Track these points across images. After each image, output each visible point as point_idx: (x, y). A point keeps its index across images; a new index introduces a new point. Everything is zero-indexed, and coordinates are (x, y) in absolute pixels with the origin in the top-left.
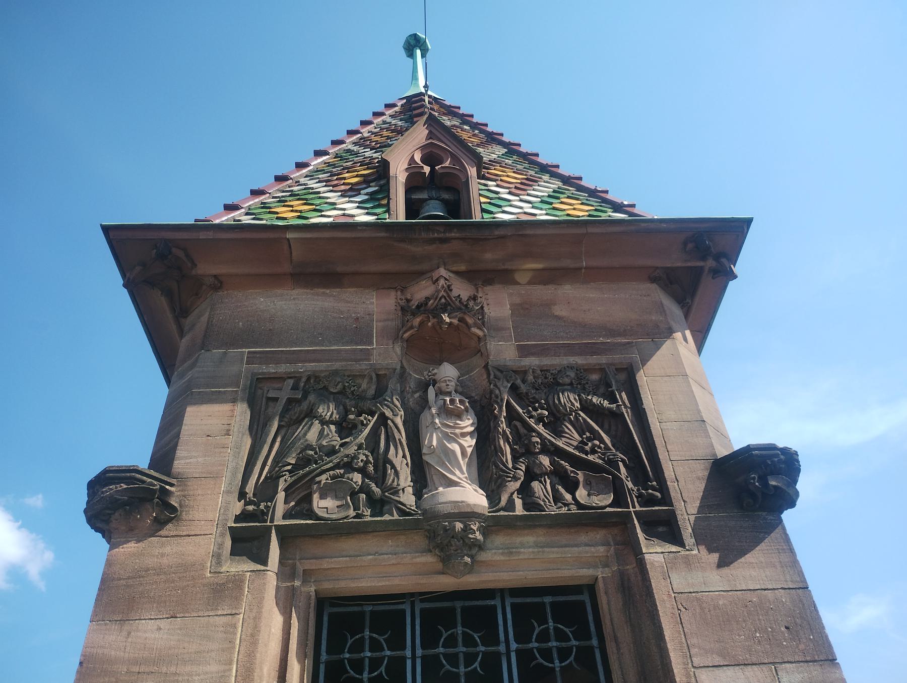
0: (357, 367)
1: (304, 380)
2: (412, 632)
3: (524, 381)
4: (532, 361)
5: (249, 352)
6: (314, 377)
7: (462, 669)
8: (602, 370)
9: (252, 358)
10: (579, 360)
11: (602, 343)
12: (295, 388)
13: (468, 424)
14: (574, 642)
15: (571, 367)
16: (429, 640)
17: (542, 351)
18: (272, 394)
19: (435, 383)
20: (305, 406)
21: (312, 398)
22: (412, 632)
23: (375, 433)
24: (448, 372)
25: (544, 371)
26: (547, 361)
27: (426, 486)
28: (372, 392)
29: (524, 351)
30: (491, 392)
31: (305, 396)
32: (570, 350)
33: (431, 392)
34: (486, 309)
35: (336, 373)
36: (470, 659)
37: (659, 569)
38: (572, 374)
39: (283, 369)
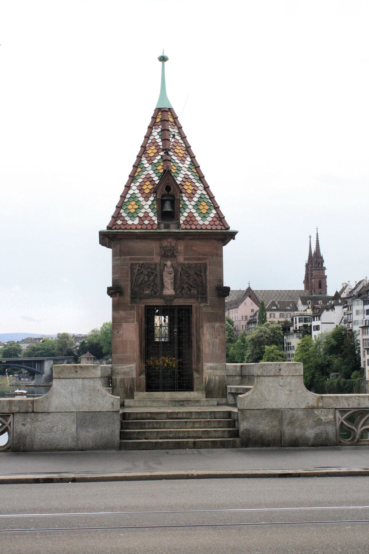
0: (151, 262)
1: (140, 265)
2: (176, 312)
3: (184, 266)
4: (186, 262)
5: (130, 258)
6: (143, 264)
7: (150, 326)
8: (200, 264)
9: (131, 259)
10: (196, 262)
11: (202, 258)
12: (139, 267)
13: (221, 435)
14: (180, 315)
15: (194, 264)
16: (179, 313)
17: (189, 259)
18: (135, 267)
19: (166, 265)
20: (141, 271)
21: (143, 269)
22: (176, 312)
23: (155, 277)
24: (169, 263)
25: (188, 264)
26: (189, 262)
27: (164, 288)
28: (154, 268)
29: (185, 259)
30: (177, 269)
31: (141, 269)
32: (195, 259)
33: (166, 267)
34: (178, 248)
35: (147, 263)
36: (182, 314)
37: (70, 387)
38: (194, 265)
39: (137, 262)
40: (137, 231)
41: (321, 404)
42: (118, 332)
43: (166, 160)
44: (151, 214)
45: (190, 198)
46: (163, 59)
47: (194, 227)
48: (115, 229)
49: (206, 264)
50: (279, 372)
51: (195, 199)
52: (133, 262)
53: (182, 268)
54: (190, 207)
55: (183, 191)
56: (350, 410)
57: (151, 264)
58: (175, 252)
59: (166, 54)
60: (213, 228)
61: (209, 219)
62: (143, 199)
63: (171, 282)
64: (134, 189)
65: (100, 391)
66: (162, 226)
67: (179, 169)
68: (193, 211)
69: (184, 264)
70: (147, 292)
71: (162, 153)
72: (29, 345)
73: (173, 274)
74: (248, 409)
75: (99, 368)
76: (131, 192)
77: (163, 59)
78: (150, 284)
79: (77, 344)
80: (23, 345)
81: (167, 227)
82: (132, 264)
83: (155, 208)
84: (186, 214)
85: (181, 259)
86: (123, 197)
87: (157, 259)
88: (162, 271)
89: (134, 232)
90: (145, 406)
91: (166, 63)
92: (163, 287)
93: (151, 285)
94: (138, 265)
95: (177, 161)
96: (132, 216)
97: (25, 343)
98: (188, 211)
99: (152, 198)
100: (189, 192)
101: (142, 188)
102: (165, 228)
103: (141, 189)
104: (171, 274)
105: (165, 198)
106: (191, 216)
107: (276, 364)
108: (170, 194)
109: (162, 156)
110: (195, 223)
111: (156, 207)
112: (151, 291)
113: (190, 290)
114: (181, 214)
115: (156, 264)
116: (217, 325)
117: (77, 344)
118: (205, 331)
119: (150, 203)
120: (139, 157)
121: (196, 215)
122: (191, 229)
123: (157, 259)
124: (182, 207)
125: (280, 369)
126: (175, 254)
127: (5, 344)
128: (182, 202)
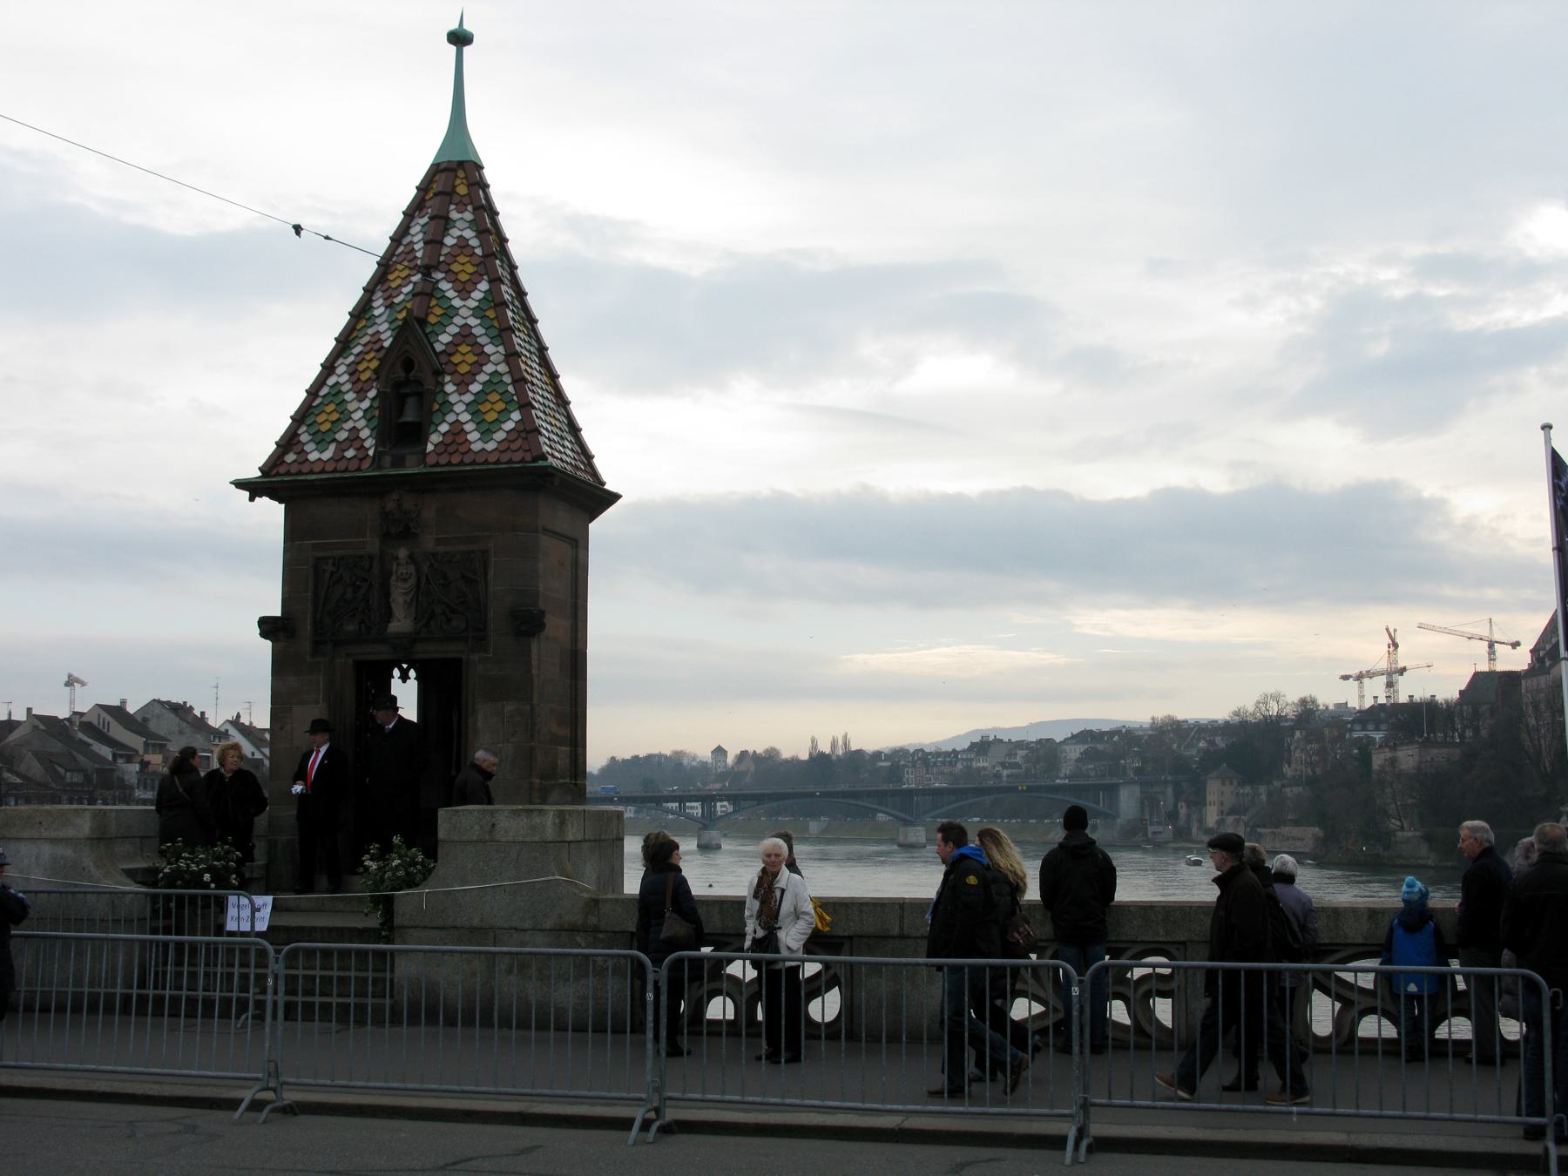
4: (441, 549)
12: (334, 564)
24: (403, 553)
29: (439, 542)
40: (314, 477)
41: (593, 920)
42: (282, 728)
43: (427, 293)
44: (365, 433)
45: (463, 386)
46: (460, 39)
47: (456, 459)
48: (278, 474)
49: (485, 552)
50: (490, 832)
51: (475, 388)
52: (320, 554)
53: (432, 564)
54: (460, 411)
55: (448, 368)
56: (1338, 951)
57: (361, 557)
58: (412, 525)
59: (467, 27)
60: (477, 461)
61: (500, 436)
62: (455, 388)
63: (405, 602)
64: (341, 376)
65: (86, 870)
66: (387, 460)
67: (450, 313)
68: (465, 417)
69: (434, 554)
70: (350, 628)
71: (417, 278)
72: (1086, 746)
73: (412, 581)
74: (412, 927)
75: (87, 816)
76: (331, 381)
77: (460, 39)
78: (357, 609)
79: (1201, 745)
80: (1073, 747)
81: (399, 462)
82: (318, 560)
83: (374, 416)
84: (444, 428)
85: (428, 542)
86: (313, 392)
87: (372, 545)
88: (386, 576)
89: (306, 480)
90: (320, 911)
91: (466, 49)
92: (389, 615)
93: (360, 609)
94: (331, 561)
95: (451, 294)
96: (321, 441)
97: (1076, 743)
98: (451, 418)
99: (372, 393)
100: (464, 369)
101: (450, 361)
102: (394, 465)
103: (353, 372)
104: (405, 580)
105: (407, 390)
106: (457, 430)
107: (484, 811)
108: (412, 379)
109: (415, 283)
110: (463, 449)
111: (377, 413)
112: (360, 624)
113: (449, 620)
114: (432, 428)
115: (371, 558)
116: (510, 707)
117: (1201, 745)
118: (480, 724)
119: (366, 404)
120: (369, 290)
121: (469, 427)
122: (449, 464)
123: (372, 545)
124: (439, 410)
125: (493, 825)
126: (413, 530)
127: (1032, 745)
128: (440, 399)
